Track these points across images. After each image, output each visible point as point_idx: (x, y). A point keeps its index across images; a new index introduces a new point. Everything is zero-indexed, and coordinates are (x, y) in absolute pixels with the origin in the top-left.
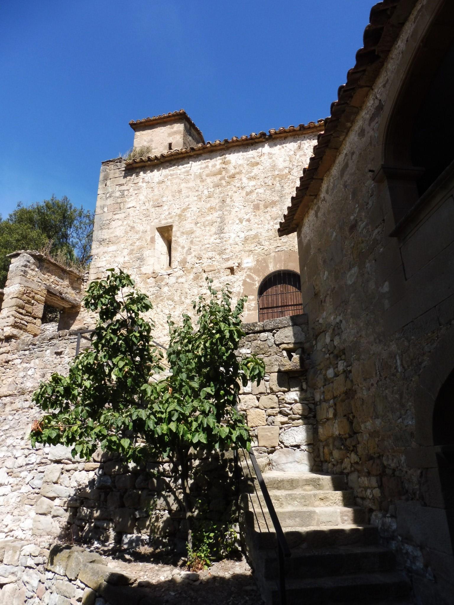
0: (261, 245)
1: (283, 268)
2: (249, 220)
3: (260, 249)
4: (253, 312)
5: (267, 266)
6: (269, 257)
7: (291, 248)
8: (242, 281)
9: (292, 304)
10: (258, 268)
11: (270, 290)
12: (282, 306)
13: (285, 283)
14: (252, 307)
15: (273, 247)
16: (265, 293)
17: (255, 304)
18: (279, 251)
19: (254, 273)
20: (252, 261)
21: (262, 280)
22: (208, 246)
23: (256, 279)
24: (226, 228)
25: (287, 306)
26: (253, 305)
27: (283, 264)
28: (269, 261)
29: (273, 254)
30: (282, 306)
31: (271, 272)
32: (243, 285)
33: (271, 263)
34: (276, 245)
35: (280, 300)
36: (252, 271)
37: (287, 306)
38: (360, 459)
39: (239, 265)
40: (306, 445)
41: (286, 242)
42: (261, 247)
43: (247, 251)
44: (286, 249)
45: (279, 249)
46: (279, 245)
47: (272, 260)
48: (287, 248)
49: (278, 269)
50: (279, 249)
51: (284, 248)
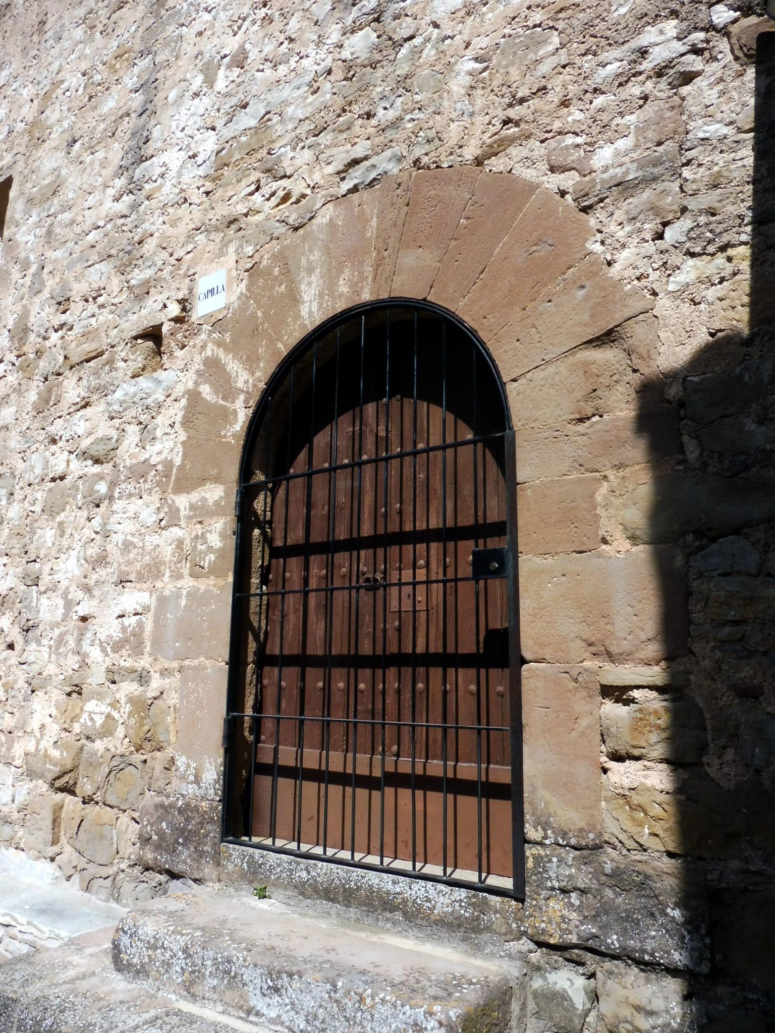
0: (276, 179)
1: (366, 296)
2: (240, 61)
3: (274, 200)
4: (211, 581)
5: (294, 298)
6: (304, 238)
7: (418, 152)
8: (184, 402)
9: (434, 523)
10: (253, 316)
11: (321, 440)
12: (377, 542)
13: (402, 389)
14: (210, 549)
15: (330, 169)
16: (299, 465)
17: (223, 536)
18: (355, 189)
19: (232, 348)
20: (230, 284)
21: (262, 386)
22: (91, 237)
23: (240, 384)
24: (156, 133)
25: (402, 538)
26: (215, 541)
27: (369, 270)
28: (304, 262)
29: (325, 215)
30: (377, 542)
31: (310, 328)
32: (186, 422)
33: (310, 270)
34: (341, 157)
35: (368, 500)
36: (227, 337)
37: (402, 538)
38: (674, 13)
39: (184, 309)
40: (662, 761)
41: (395, 124)
42: (275, 185)
43: (217, 229)
44: (393, 168)
45: (356, 176)
46: (359, 151)
47: (316, 256)
48: (400, 159)
49: (341, 306)
50: (356, 176)
51: (384, 163)
